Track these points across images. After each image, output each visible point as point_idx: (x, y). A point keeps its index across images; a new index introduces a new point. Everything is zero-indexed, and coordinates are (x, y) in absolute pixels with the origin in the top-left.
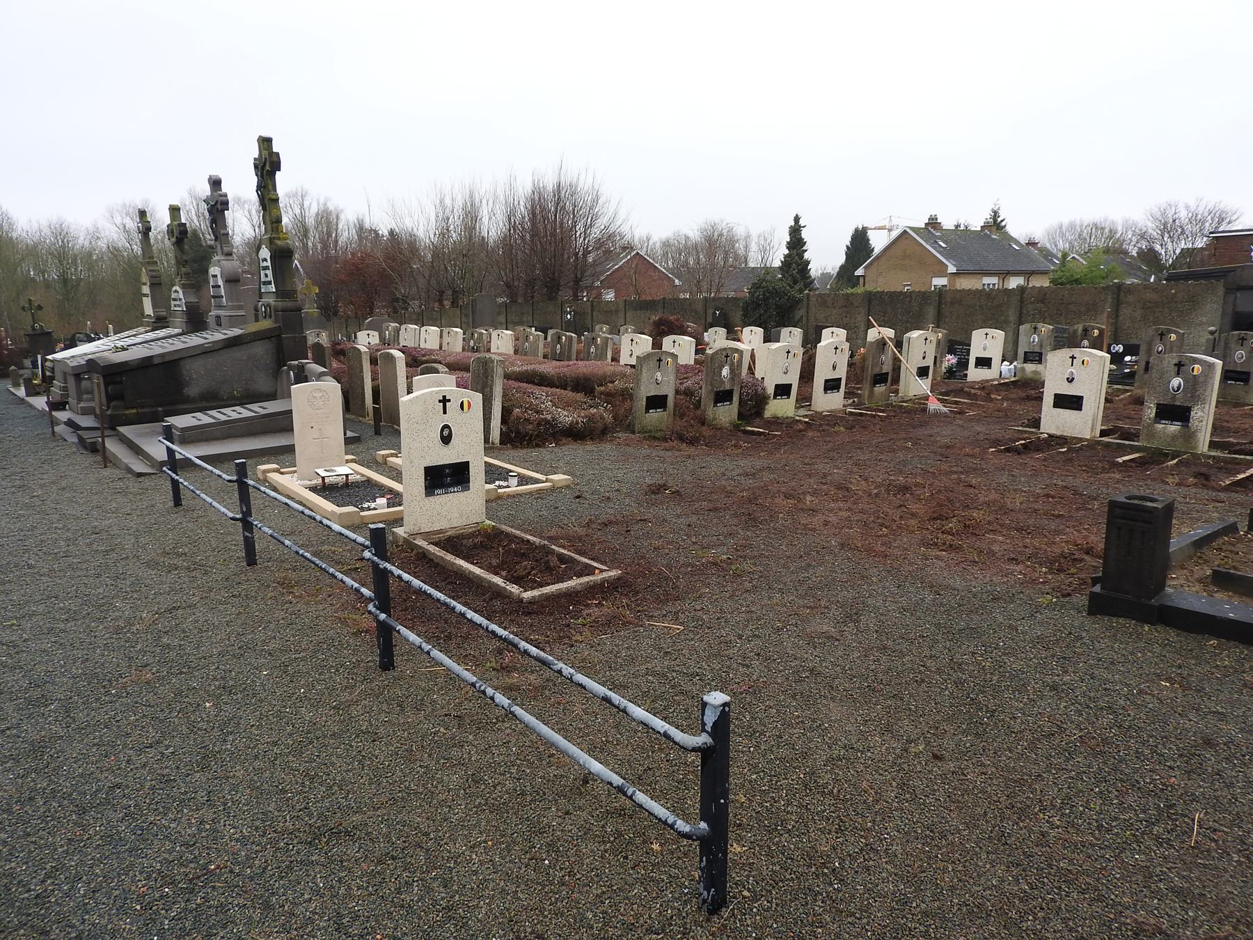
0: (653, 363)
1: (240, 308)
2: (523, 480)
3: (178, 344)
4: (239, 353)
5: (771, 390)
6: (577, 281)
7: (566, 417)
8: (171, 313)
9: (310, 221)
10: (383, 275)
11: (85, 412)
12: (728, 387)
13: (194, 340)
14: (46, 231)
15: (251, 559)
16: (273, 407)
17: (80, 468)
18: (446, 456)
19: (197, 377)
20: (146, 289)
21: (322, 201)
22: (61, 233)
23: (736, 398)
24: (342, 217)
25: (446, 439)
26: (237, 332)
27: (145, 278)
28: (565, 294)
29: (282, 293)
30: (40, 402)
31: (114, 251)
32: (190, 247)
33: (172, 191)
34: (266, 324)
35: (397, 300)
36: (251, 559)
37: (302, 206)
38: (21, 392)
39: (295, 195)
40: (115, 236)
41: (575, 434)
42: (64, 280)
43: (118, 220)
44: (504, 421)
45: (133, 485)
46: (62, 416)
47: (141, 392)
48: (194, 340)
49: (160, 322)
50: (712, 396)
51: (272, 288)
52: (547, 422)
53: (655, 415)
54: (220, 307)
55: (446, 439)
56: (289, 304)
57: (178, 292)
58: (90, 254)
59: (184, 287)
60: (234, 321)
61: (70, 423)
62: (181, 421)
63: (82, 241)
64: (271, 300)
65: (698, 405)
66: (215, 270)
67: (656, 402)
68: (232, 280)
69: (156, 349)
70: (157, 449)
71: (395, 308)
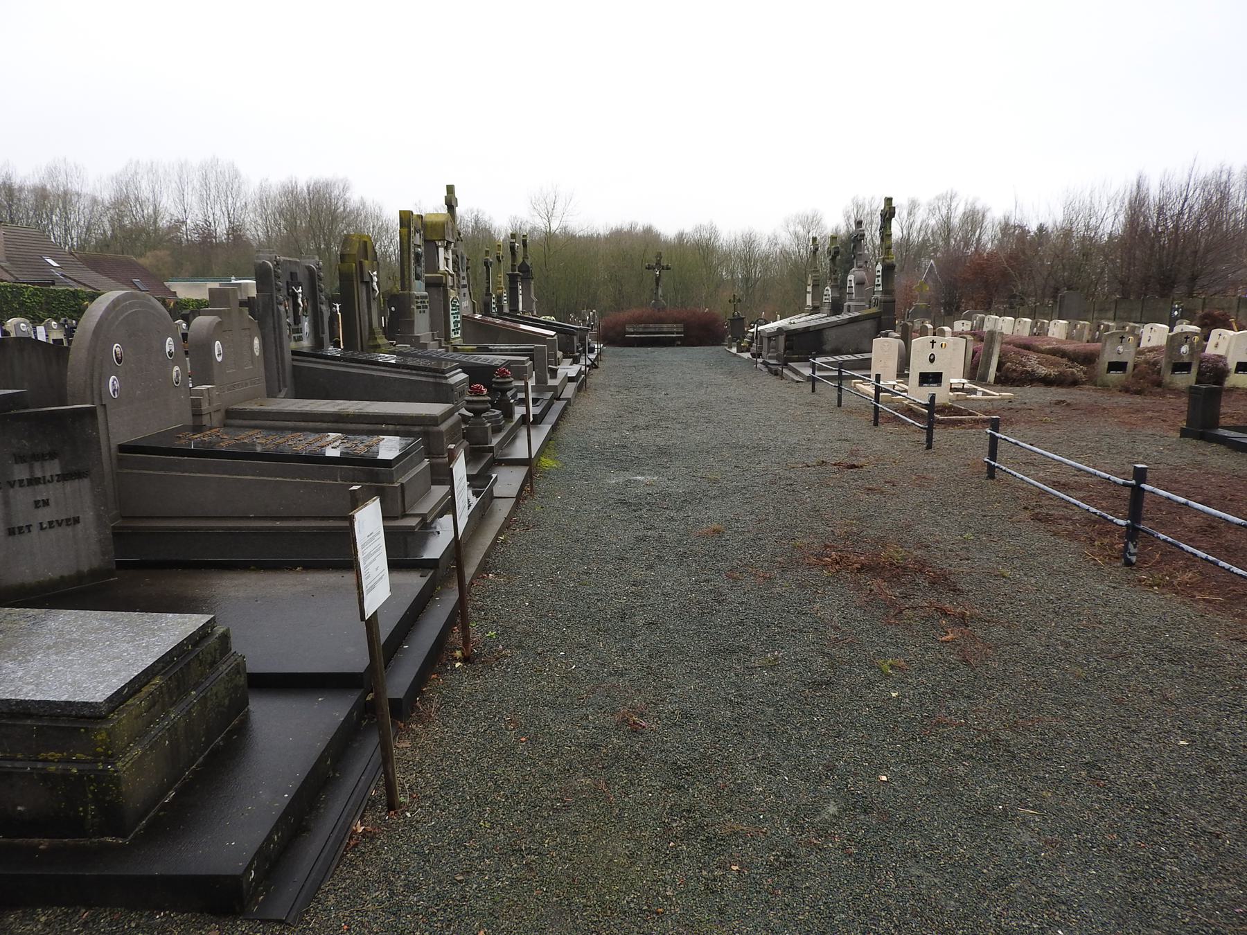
0: (1117, 339)
1: (862, 300)
2: (984, 394)
3: (824, 321)
4: (856, 327)
5: (1232, 366)
6: (1194, 278)
7: (1043, 371)
8: (822, 304)
9: (956, 221)
10: (1004, 274)
11: (770, 358)
12: (1186, 360)
13: (834, 319)
14: (740, 240)
15: (839, 405)
16: (866, 356)
17: (773, 381)
18: (931, 369)
19: (831, 338)
20: (809, 289)
21: (970, 200)
22: (750, 242)
23: (1194, 370)
24: (988, 215)
25: (932, 361)
26: (857, 314)
27: (810, 281)
28: (1179, 291)
29: (886, 292)
30: (747, 355)
31: (785, 254)
32: (846, 249)
33: (834, 221)
34: (874, 310)
35: (1014, 296)
36: (839, 405)
37: (949, 208)
38: (734, 350)
39: (944, 198)
40: (787, 243)
41: (1047, 381)
42: (747, 279)
43: (792, 229)
44: (999, 369)
45: (795, 385)
46: (760, 360)
47: (802, 345)
48: (834, 319)
49: (815, 310)
50: (1170, 366)
51: (880, 288)
52: (1027, 372)
53: (1115, 376)
54: (851, 300)
55: (932, 361)
56: (888, 298)
57: (828, 290)
58: (767, 258)
59: (832, 287)
60: (857, 308)
61: (764, 363)
62: (819, 361)
63: (763, 246)
64: (878, 296)
65: (1159, 372)
66: (851, 277)
67: (1118, 366)
68: (860, 283)
69: (812, 323)
70: (807, 372)
71: (1011, 304)
